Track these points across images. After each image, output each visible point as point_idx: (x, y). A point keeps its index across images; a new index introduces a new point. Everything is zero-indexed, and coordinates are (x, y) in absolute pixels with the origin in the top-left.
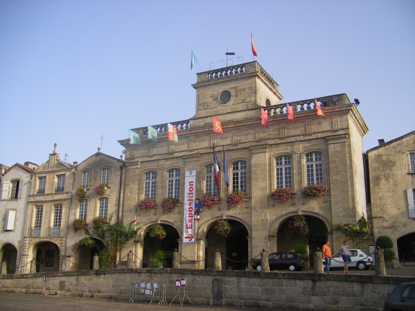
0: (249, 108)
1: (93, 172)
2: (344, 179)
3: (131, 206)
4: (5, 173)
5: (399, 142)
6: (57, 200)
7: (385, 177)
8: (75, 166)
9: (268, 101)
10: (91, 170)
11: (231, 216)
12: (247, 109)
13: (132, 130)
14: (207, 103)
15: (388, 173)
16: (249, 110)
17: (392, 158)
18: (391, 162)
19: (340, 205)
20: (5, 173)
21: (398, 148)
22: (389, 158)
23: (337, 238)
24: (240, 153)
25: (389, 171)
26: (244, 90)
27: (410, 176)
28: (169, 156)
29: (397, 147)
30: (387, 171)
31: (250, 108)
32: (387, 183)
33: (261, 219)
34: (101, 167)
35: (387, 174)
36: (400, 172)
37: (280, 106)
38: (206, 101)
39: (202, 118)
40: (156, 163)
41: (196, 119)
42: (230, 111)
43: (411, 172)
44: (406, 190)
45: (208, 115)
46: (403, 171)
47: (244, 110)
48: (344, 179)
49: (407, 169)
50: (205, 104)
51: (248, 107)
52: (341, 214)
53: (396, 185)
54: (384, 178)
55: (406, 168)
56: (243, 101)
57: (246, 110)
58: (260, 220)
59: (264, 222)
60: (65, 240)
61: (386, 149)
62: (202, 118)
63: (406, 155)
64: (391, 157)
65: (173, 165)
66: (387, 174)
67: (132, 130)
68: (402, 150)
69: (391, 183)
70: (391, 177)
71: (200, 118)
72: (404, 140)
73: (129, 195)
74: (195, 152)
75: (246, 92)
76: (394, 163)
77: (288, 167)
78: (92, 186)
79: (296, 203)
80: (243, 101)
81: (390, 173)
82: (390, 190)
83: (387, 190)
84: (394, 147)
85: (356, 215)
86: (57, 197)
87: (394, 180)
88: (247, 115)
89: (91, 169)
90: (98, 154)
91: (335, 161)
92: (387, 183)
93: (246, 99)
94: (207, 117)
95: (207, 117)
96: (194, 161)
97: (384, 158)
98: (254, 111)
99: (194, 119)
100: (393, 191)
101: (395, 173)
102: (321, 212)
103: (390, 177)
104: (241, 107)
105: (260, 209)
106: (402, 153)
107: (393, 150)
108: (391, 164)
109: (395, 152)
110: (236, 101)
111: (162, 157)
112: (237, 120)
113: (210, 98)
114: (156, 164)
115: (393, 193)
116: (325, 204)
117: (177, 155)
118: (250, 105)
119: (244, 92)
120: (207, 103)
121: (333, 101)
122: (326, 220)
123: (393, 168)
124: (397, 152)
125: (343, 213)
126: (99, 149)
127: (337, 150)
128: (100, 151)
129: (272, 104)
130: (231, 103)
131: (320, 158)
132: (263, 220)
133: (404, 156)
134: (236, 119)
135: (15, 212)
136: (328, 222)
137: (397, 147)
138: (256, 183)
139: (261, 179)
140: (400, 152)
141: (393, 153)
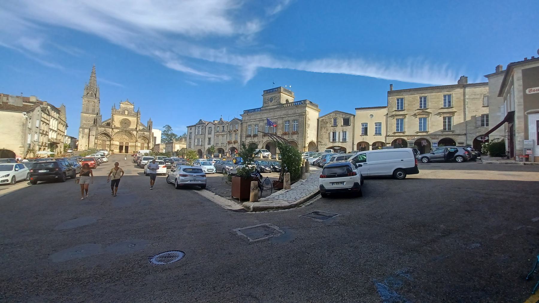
3: (522, 136)
4: (207, 125)
6: (223, 134)
8: (227, 123)
9: (287, 101)
13: (384, 116)
20: (207, 125)
21: (329, 117)
28: (254, 120)
43: (343, 125)
44: (330, 133)
60: (467, 143)
67: (384, 116)
74: (262, 119)
77: (484, 126)
85: (516, 141)
86: (223, 133)
95: (266, 107)
99: (262, 107)
102: (296, 140)
114: (251, 123)
129: (290, 102)
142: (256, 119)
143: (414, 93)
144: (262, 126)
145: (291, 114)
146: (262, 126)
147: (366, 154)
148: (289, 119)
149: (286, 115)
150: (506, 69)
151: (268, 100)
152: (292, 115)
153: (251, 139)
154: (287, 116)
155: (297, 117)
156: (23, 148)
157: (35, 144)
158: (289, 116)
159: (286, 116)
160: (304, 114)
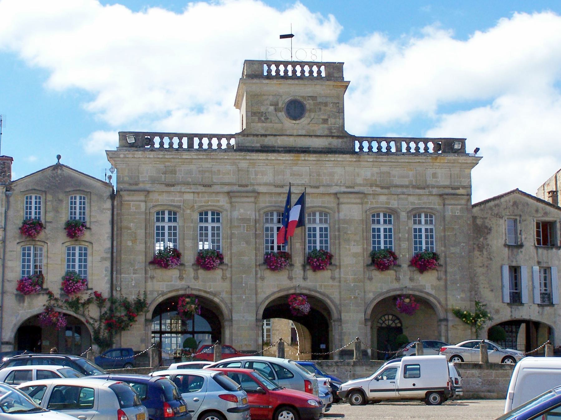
0: (333, 134)
1: (49, 197)
2: (463, 254)
5: (497, 202)
7: (479, 248)
10: (46, 194)
11: (310, 290)
12: (330, 134)
14: (265, 113)
15: (483, 243)
16: (333, 137)
17: (488, 223)
18: (486, 227)
19: (458, 285)
21: (496, 211)
22: (484, 222)
23: (453, 326)
24: (321, 200)
25: (484, 239)
26: (326, 104)
27: (507, 249)
29: (494, 208)
30: (481, 239)
31: (336, 134)
32: (480, 255)
33: (354, 297)
34: (67, 190)
35: (481, 243)
36: (495, 242)
37: (378, 139)
38: (263, 109)
39: (257, 135)
40: (176, 197)
41: (248, 135)
42: (304, 132)
45: (266, 133)
46: (500, 241)
47: (327, 136)
48: (463, 254)
49: (504, 239)
50: (261, 114)
51: (332, 133)
52: (459, 297)
53: (491, 259)
54: (477, 249)
55: (502, 238)
56: (325, 121)
57: (330, 136)
58: (353, 297)
59: (359, 301)
61: (482, 210)
62: (257, 135)
63: (504, 220)
64: (487, 221)
65: (210, 203)
66: (481, 243)
68: (500, 214)
69: (485, 256)
70: (486, 247)
71: (254, 135)
72: (503, 200)
73: (131, 244)
75: (328, 108)
76: (490, 229)
78: (50, 222)
79: (401, 278)
80: (325, 121)
81: (485, 242)
82: (483, 265)
83: (480, 265)
84: (491, 208)
87: (488, 252)
88: (330, 144)
89: (46, 192)
90: (58, 166)
91: (453, 229)
92: (480, 255)
93: (329, 119)
94: (266, 136)
95: (266, 136)
96: (248, 202)
97: (479, 222)
98: (340, 140)
100: (487, 267)
101: (490, 243)
102: (433, 292)
103: (484, 248)
104: (321, 129)
105: (352, 282)
106: (500, 217)
107: (490, 212)
108: (486, 231)
109: (491, 215)
110: (313, 120)
111: (190, 188)
112: (315, 149)
113: (271, 105)
115: (486, 269)
116: (438, 283)
117: (217, 188)
118: (335, 129)
119: (326, 108)
120: (265, 113)
121: (460, 148)
122: (440, 303)
123: (488, 236)
124: (494, 215)
125: (462, 296)
126: (59, 157)
127: (457, 214)
128: (61, 161)
130: (304, 121)
131: (431, 221)
132: (357, 297)
133: (502, 222)
134: (313, 148)
135: (509, 302)
136: (442, 306)
137: (494, 208)
138: (347, 247)
139: (354, 241)
140: (498, 216)
141: (489, 216)
142: (246, 186)
143: (246, 156)
144: (249, 220)
145: (407, 187)
146: (252, 224)
147: (419, 365)
148: (394, 204)
149: (382, 188)
150: (346, 129)
151: (276, 105)
152: (411, 191)
153: (181, 278)
154: (385, 191)
155: (434, 203)
156: (361, 206)
157: (550, 184)
158: (393, 190)
159: (378, 190)
160: (461, 191)
